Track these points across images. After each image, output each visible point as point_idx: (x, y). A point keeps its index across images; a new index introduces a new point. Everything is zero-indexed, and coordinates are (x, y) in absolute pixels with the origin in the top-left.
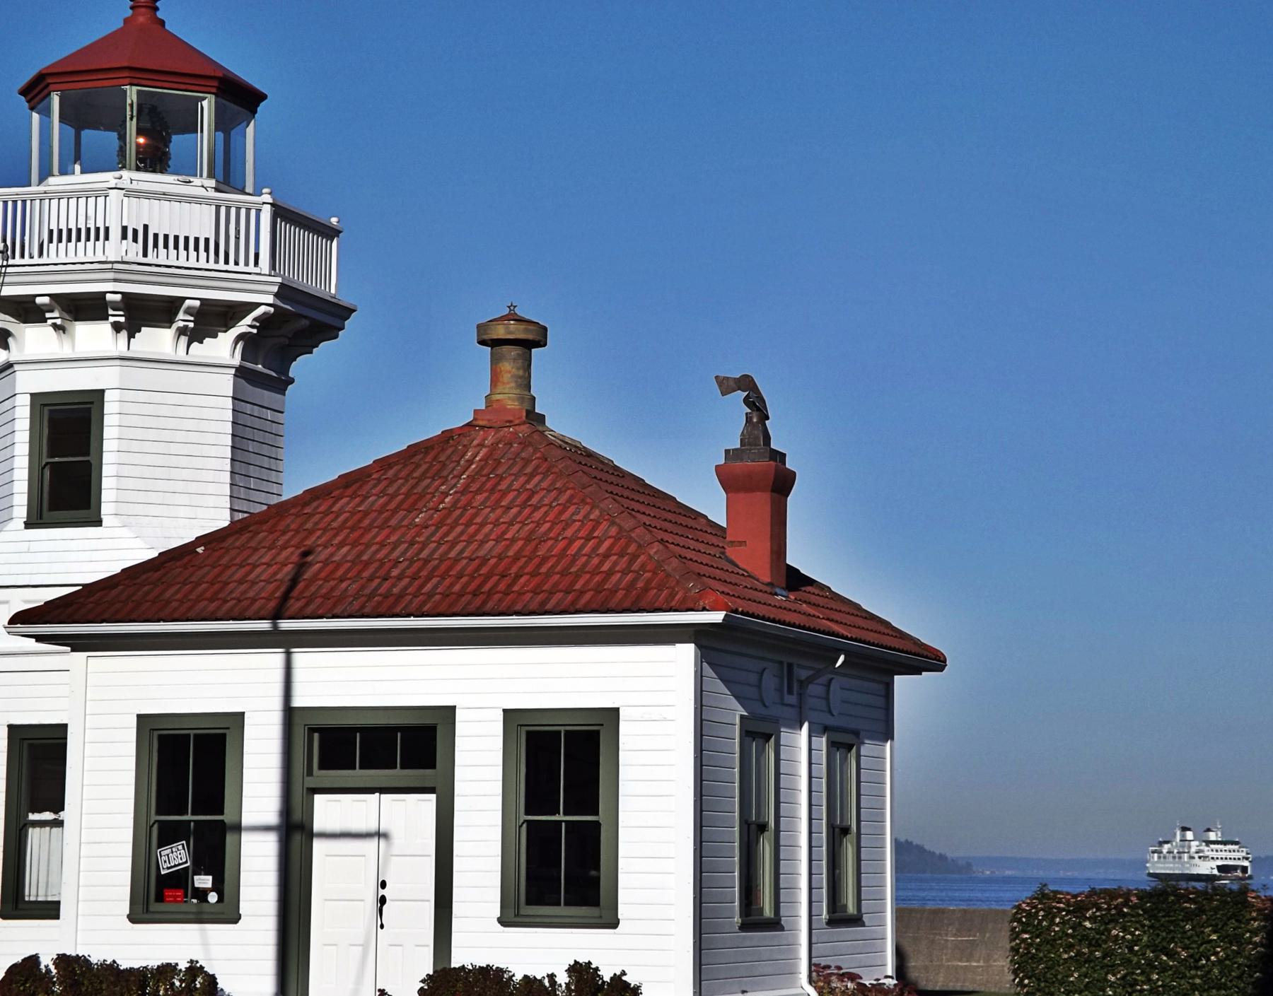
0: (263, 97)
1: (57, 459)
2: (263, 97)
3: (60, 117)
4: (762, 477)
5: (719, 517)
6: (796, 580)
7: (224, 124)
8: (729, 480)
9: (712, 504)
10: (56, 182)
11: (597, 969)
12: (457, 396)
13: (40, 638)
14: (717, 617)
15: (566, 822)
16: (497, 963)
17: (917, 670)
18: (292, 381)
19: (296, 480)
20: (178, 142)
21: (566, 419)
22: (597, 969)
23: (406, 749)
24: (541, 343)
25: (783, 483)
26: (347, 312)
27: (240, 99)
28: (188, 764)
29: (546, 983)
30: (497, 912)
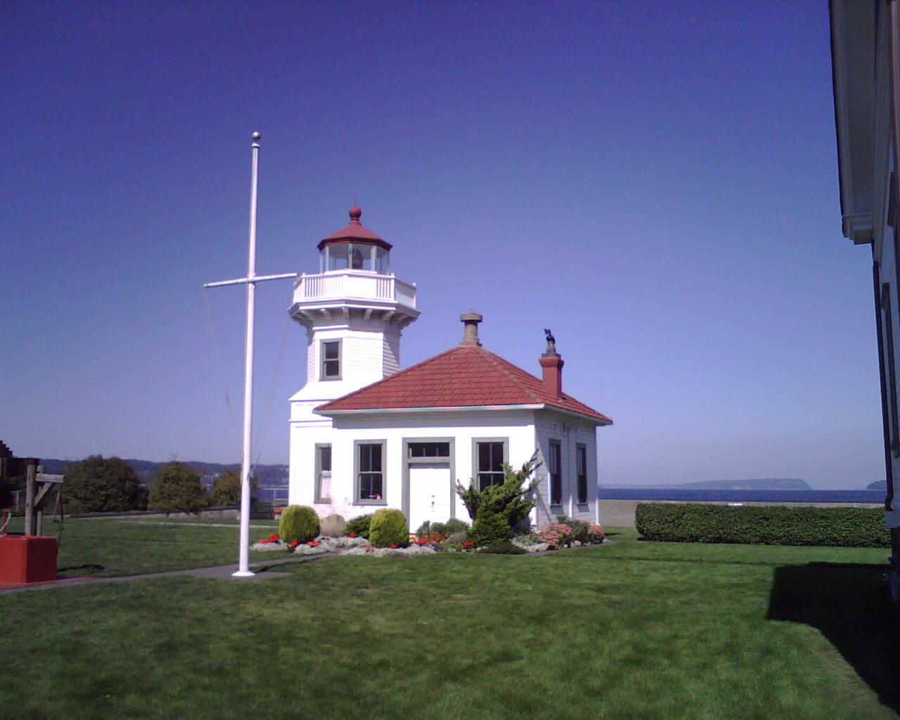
0: (392, 246)
1: (364, 472)
2: (392, 246)
3: (330, 253)
4: (555, 364)
5: (540, 377)
6: (564, 397)
7: (379, 256)
8: (544, 364)
9: (537, 372)
10: (327, 273)
11: (11, 452)
12: (454, 338)
13: (323, 415)
14: (541, 406)
15: (493, 474)
16: (96, 453)
17: (603, 425)
18: (401, 335)
19: (403, 367)
20: (365, 262)
21: (489, 346)
22: (11, 452)
23: (438, 451)
24: (480, 321)
25: (560, 365)
26: (419, 313)
27: (385, 246)
28: (371, 456)
29: (277, 480)
30: (313, 500)
